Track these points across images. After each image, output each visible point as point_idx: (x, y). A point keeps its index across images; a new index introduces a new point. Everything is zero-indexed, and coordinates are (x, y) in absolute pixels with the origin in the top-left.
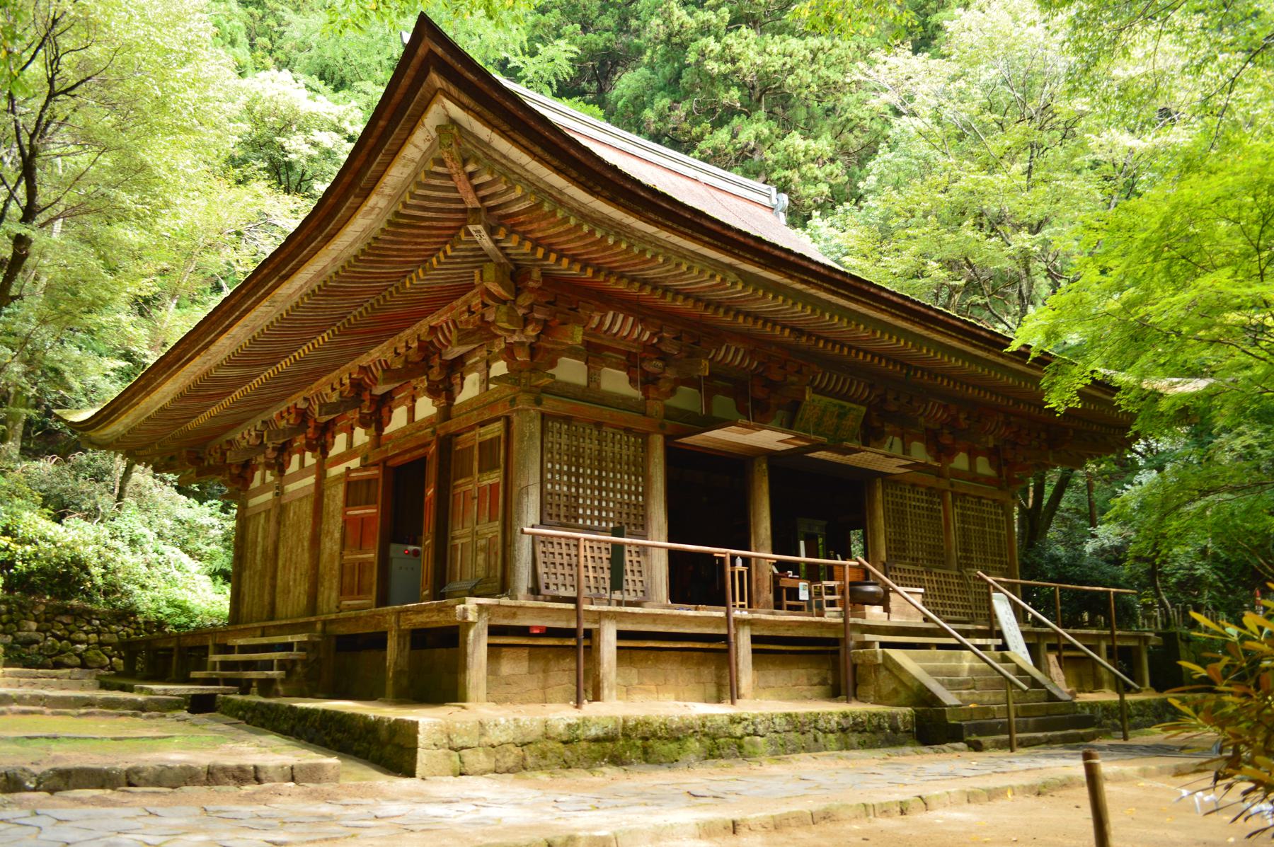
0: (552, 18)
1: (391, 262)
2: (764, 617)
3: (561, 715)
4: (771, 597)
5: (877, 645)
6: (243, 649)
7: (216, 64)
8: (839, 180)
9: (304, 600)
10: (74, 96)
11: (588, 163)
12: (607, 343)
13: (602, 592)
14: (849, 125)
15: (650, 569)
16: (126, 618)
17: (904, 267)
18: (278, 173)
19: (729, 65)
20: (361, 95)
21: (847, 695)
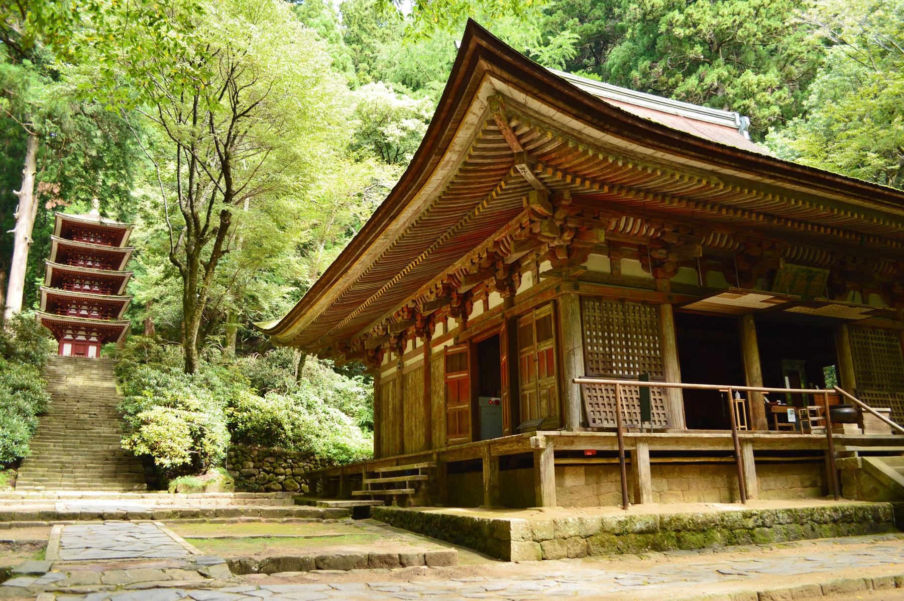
0: (557, 17)
1: (464, 198)
2: (762, 436)
3: (614, 514)
4: (765, 421)
5: (856, 454)
6: (385, 475)
7: (335, 83)
8: (787, 101)
10: (248, 116)
11: (598, 108)
12: (623, 240)
13: (635, 423)
14: (791, 59)
15: (670, 404)
16: (308, 458)
17: (847, 160)
18: (381, 152)
19: (692, 29)
20: (431, 91)
21: (834, 494)
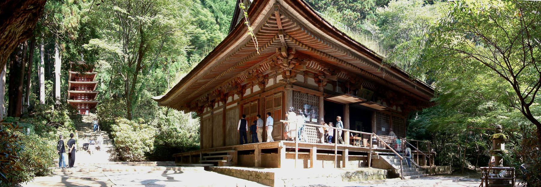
9: (222, 142)
